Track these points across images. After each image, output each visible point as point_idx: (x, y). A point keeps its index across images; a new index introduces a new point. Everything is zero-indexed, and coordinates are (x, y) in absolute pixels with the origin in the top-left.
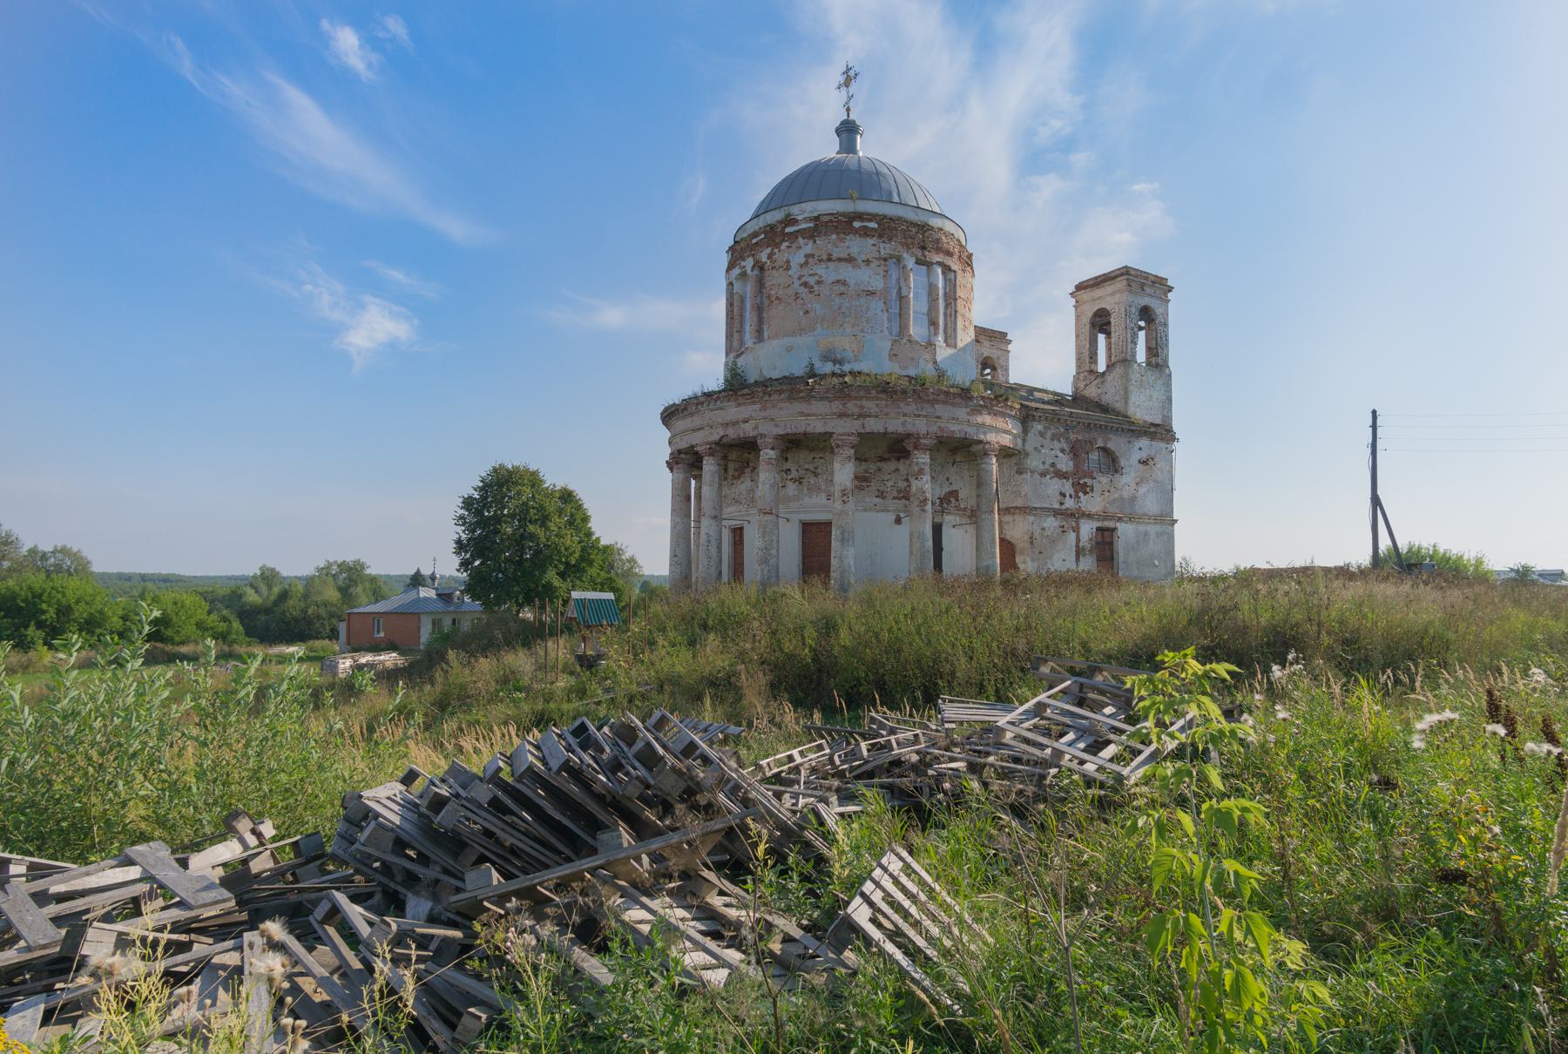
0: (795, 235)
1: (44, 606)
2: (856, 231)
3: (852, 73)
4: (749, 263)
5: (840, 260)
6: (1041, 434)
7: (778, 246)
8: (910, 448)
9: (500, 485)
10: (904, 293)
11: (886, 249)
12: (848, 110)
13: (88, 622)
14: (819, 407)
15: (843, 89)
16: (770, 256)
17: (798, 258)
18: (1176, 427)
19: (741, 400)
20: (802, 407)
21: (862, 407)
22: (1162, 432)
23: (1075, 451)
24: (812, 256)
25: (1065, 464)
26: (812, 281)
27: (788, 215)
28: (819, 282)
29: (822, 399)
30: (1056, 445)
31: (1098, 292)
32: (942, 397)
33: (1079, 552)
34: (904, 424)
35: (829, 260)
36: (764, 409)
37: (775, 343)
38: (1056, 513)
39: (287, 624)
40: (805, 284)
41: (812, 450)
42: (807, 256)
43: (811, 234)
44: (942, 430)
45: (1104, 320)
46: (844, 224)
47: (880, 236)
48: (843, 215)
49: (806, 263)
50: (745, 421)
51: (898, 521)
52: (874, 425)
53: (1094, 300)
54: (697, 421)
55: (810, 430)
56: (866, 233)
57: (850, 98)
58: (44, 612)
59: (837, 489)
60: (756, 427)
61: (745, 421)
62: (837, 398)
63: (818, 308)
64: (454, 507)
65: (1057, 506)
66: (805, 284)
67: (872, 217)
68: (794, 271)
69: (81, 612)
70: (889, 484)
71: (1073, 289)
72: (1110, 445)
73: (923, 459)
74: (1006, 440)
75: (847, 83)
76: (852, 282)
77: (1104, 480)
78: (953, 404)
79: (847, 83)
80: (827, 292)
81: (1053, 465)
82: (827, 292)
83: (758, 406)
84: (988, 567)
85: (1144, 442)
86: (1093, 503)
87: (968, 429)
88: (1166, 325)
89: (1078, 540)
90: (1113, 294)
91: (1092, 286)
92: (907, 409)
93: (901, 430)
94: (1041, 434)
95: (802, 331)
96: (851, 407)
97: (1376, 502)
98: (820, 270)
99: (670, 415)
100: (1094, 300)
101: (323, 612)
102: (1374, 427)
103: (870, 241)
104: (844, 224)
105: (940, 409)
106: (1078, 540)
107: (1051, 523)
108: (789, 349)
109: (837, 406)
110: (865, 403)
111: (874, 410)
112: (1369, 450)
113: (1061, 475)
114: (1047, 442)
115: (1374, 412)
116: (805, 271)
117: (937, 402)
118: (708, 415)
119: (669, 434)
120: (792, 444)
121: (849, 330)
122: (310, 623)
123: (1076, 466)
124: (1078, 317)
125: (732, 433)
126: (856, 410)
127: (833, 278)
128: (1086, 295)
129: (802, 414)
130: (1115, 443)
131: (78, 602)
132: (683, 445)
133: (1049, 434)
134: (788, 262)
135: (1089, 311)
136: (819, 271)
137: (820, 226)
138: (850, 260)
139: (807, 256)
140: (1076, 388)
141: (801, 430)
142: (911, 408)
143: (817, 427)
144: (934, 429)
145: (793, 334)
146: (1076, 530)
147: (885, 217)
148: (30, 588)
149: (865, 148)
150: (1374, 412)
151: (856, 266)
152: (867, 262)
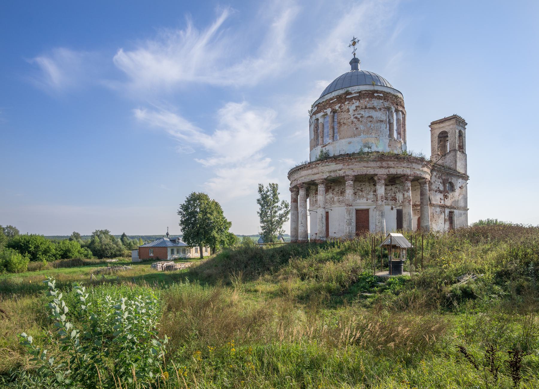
0: (352, 99)
1: (30, 245)
2: (376, 97)
3: (356, 40)
4: (329, 111)
5: (370, 108)
7: (344, 103)
8: (404, 180)
9: (195, 200)
10: (391, 122)
11: (386, 104)
12: (354, 54)
13: (45, 251)
14: (372, 164)
15: (352, 47)
16: (340, 107)
17: (353, 107)
18: (468, 173)
19: (338, 162)
20: (365, 164)
21: (388, 164)
22: (465, 177)
23: (444, 183)
24: (359, 107)
26: (359, 116)
27: (347, 92)
28: (362, 117)
29: (373, 161)
31: (442, 125)
32: (415, 161)
33: (445, 220)
34: (403, 170)
35: (366, 108)
36: (348, 165)
37: (343, 141)
39: (96, 251)
40: (356, 118)
41: (360, 182)
42: (356, 107)
43: (358, 98)
44: (415, 173)
45: (446, 135)
46: (371, 94)
47: (385, 99)
48: (370, 91)
49: (356, 109)
50: (340, 170)
51: (392, 209)
52: (393, 171)
53: (440, 128)
54: (315, 171)
55: (368, 173)
56: (379, 98)
57: (355, 50)
58: (30, 248)
59: (379, 196)
60: (345, 172)
61: (340, 170)
62: (379, 161)
63: (361, 127)
64: (178, 208)
66: (356, 118)
67: (381, 92)
68: (351, 112)
69: (43, 247)
70: (389, 195)
71: (430, 124)
72: (452, 181)
73: (409, 184)
75: (354, 44)
76: (374, 117)
79: (354, 44)
80: (365, 121)
81: (438, 188)
82: (365, 121)
84: (427, 226)
87: (422, 173)
88: (465, 137)
90: (448, 126)
91: (439, 123)
93: (402, 173)
95: (355, 136)
96: (384, 164)
98: (362, 112)
100: (440, 128)
101: (108, 247)
103: (381, 101)
104: (371, 94)
105: (414, 165)
107: (438, 209)
108: (350, 143)
109: (379, 164)
111: (393, 165)
113: (441, 192)
114: (437, 179)
116: (356, 113)
117: (413, 162)
120: (359, 179)
121: (374, 135)
122: (103, 251)
124: (432, 135)
125: (333, 175)
127: (367, 115)
128: (435, 126)
129: (365, 167)
130: (454, 180)
131: (41, 244)
134: (348, 109)
135: (437, 132)
136: (362, 113)
137: (361, 95)
138: (374, 108)
139: (356, 107)
141: (364, 173)
142: (405, 165)
143: (371, 172)
144: (412, 173)
145: (351, 137)
147: (385, 92)
148: (25, 239)
149: (361, 68)
151: (376, 111)
152: (380, 109)
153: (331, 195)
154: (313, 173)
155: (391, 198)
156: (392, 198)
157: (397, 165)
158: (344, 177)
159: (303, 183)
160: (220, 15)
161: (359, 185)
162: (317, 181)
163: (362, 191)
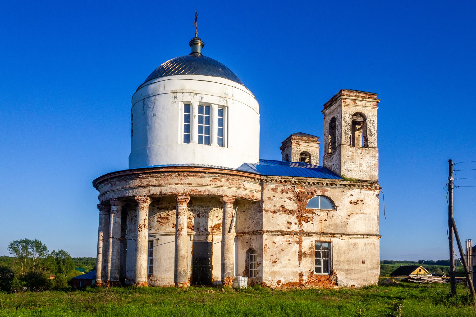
6: (273, 190)
23: (299, 198)
25: (292, 205)
33: (301, 255)
38: (283, 233)
65: (285, 229)
77: (323, 214)
81: (282, 207)
83: (110, 185)
89: (301, 248)
93: (169, 192)
94: (273, 190)
97: (451, 223)
102: (132, 135)
106: (301, 248)
110: (150, 179)
111: (156, 183)
113: (291, 212)
114: (278, 194)
115: (450, 161)
133: (279, 189)
146: (300, 243)
150: (450, 161)
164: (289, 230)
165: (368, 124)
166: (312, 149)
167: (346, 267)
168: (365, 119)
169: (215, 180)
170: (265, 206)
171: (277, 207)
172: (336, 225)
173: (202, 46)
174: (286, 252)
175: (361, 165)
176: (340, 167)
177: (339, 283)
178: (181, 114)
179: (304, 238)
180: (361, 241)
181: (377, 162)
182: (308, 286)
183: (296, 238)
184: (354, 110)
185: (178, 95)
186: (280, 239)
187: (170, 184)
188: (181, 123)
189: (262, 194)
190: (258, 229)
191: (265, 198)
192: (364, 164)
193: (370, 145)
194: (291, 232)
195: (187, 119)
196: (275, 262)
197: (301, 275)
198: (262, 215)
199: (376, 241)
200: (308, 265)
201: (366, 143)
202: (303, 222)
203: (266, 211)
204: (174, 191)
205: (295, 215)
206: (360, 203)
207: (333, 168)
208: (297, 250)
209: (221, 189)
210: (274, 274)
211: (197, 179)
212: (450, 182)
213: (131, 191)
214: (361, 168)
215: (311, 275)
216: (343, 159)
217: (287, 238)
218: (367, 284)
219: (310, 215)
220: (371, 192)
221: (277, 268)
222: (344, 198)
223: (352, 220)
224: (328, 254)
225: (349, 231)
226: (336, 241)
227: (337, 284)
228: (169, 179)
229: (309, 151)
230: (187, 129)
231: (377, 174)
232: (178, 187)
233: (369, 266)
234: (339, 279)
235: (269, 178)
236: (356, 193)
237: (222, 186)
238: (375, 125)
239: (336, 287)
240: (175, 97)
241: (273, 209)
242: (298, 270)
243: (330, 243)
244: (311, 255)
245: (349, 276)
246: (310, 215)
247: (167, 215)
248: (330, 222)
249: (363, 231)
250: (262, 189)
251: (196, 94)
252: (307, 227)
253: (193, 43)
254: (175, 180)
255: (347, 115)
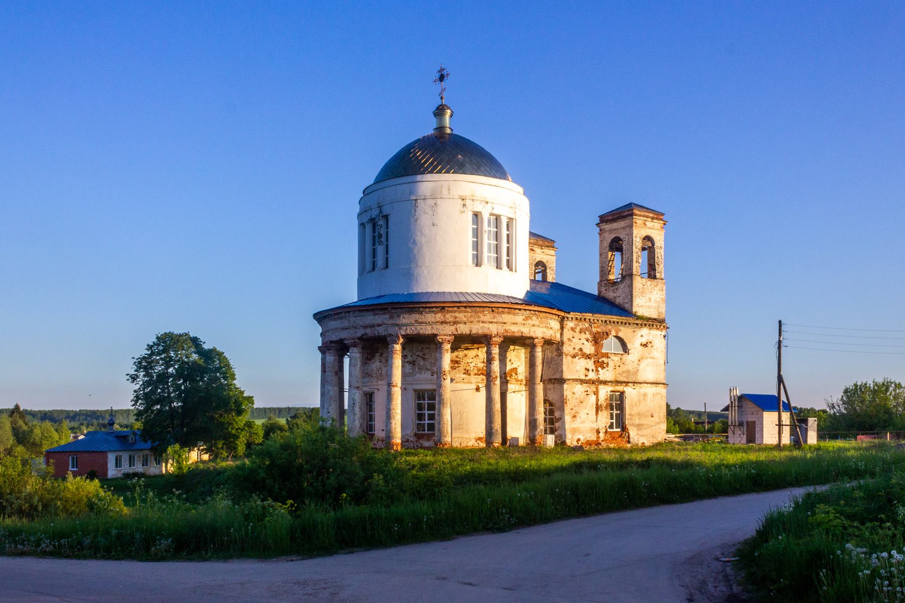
3: (445, 72)
6: (573, 329)
23: (597, 340)
25: (589, 349)
30: (583, 336)
33: (598, 408)
36: (391, 317)
38: (582, 382)
44: (506, 331)
50: (379, 325)
54: (345, 323)
61: (379, 325)
65: (583, 377)
70: (472, 365)
72: (620, 335)
74: (548, 334)
75: (442, 78)
78: (514, 314)
79: (442, 78)
81: (581, 350)
83: (387, 316)
85: (645, 331)
86: (606, 374)
89: (597, 400)
92: (483, 318)
93: (480, 332)
94: (573, 329)
96: (449, 317)
99: (321, 317)
105: (506, 317)
106: (597, 400)
110: (457, 314)
112: (777, 346)
113: (588, 357)
114: (577, 335)
115: (780, 322)
118: (352, 319)
119: (320, 331)
123: (596, 350)
126: (452, 319)
132: (334, 338)
133: (578, 329)
135: (609, 237)
140: (600, 292)
146: (596, 393)
150: (780, 322)
153: (378, 364)
154: (342, 326)
155: (476, 371)
156: (479, 370)
157: (472, 319)
158: (385, 336)
159: (331, 342)
160: (109, 461)
161: (420, 348)
162: (346, 342)
163: (424, 359)
164: (587, 378)
165: (656, 250)
166: (549, 257)
167: (637, 422)
168: (653, 244)
169: (527, 318)
170: (567, 349)
171: (576, 351)
172: (628, 371)
173: (451, 116)
174: (584, 405)
175: (650, 299)
176: (632, 301)
177: (631, 440)
178: (470, 227)
179: (601, 387)
180: (650, 390)
181: (664, 297)
182: (604, 445)
183: (593, 388)
184: (644, 232)
185: (468, 202)
186: (579, 389)
187: (483, 322)
188: (470, 239)
189: (562, 334)
190: (557, 376)
191: (565, 340)
192: (653, 299)
193: (658, 275)
194: (589, 380)
195: (477, 233)
196: (575, 416)
197: (598, 432)
198: (562, 360)
199: (662, 390)
200: (604, 419)
201: (652, 273)
202: (599, 369)
203: (566, 355)
204: (486, 331)
205: (593, 360)
206: (649, 345)
207: (619, 301)
208: (595, 403)
209: (533, 329)
210: (574, 431)
211: (511, 316)
212: (780, 342)
213: (429, 328)
214: (650, 304)
215: (606, 432)
216: (635, 293)
217: (584, 387)
218: (655, 441)
219: (605, 360)
220: (659, 332)
221: (577, 424)
222: (636, 337)
223: (642, 366)
224: (621, 407)
225: (640, 379)
226: (629, 391)
227: (629, 442)
228: (481, 315)
229: (544, 261)
230: (477, 246)
231: (664, 310)
232: (491, 326)
233: (657, 420)
234: (631, 436)
235: (572, 315)
236: (645, 334)
237: (534, 325)
238: (662, 251)
239: (629, 445)
240: (464, 205)
241: (572, 352)
242: (595, 426)
243: (622, 393)
244: (606, 408)
245: (640, 432)
246: (605, 360)
247: (457, 357)
248: (624, 368)
249: (651, 379)
250: (562, 328)
251: (487, 203)
252: (604, 375)
253: (439, 112)
254: (487, 316)
255: (638, 239)
